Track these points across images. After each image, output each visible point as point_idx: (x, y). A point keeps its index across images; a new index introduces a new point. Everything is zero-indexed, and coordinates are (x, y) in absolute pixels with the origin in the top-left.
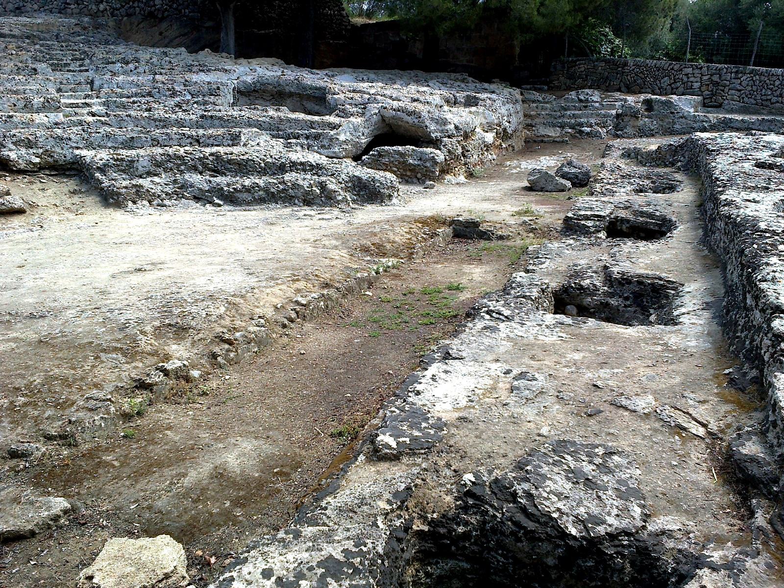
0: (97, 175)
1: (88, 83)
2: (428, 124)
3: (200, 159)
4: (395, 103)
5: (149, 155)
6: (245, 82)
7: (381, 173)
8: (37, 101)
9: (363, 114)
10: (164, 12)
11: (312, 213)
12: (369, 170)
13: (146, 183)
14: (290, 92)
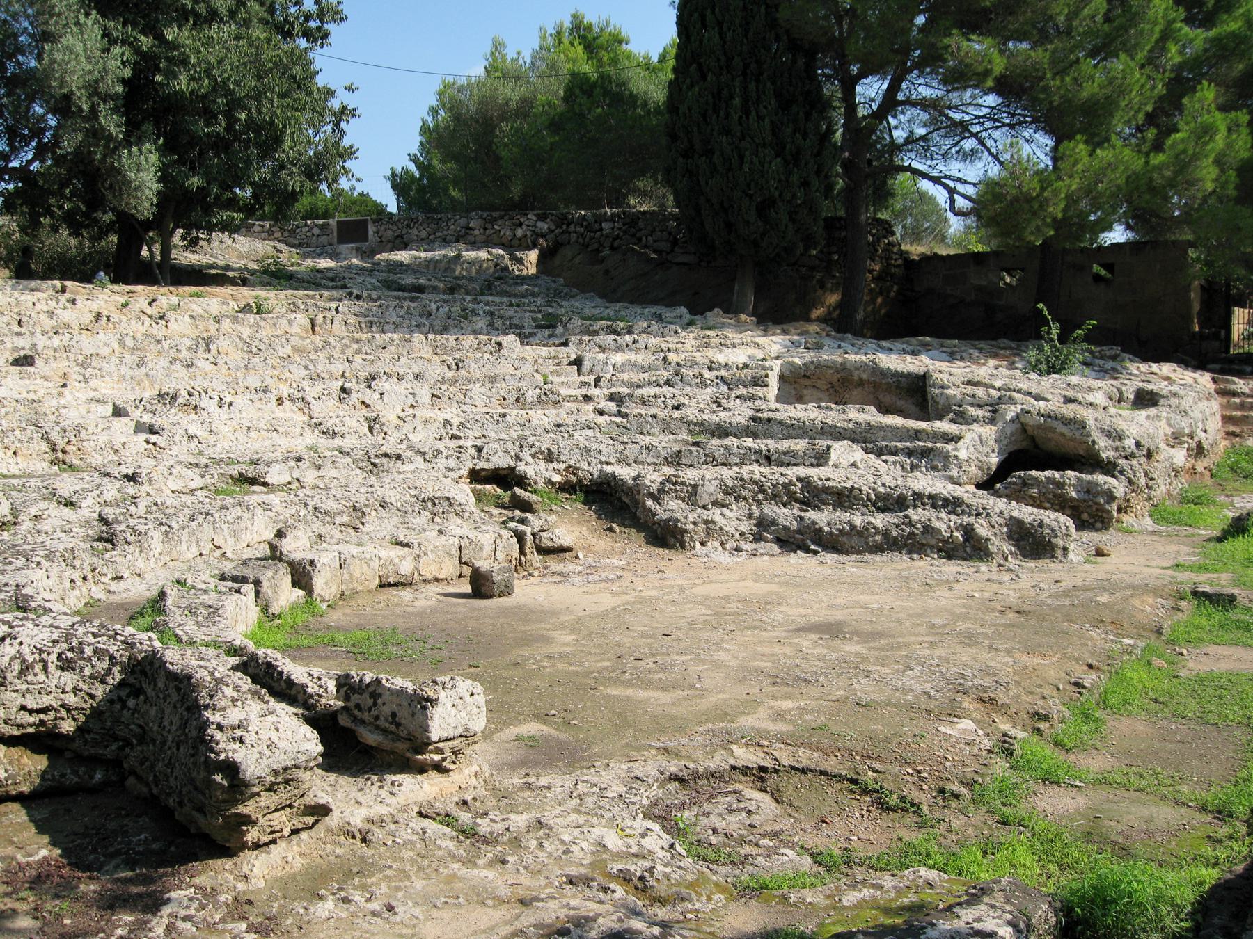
0: (649, 503)
1: (571, 364)
3: (785, 486)
4: (1042, 403)
6: (792, 364)
8: (532, 394)
9: (992, 421)
10: (614, 239)
11: (967, 570)
14: (861, 379)
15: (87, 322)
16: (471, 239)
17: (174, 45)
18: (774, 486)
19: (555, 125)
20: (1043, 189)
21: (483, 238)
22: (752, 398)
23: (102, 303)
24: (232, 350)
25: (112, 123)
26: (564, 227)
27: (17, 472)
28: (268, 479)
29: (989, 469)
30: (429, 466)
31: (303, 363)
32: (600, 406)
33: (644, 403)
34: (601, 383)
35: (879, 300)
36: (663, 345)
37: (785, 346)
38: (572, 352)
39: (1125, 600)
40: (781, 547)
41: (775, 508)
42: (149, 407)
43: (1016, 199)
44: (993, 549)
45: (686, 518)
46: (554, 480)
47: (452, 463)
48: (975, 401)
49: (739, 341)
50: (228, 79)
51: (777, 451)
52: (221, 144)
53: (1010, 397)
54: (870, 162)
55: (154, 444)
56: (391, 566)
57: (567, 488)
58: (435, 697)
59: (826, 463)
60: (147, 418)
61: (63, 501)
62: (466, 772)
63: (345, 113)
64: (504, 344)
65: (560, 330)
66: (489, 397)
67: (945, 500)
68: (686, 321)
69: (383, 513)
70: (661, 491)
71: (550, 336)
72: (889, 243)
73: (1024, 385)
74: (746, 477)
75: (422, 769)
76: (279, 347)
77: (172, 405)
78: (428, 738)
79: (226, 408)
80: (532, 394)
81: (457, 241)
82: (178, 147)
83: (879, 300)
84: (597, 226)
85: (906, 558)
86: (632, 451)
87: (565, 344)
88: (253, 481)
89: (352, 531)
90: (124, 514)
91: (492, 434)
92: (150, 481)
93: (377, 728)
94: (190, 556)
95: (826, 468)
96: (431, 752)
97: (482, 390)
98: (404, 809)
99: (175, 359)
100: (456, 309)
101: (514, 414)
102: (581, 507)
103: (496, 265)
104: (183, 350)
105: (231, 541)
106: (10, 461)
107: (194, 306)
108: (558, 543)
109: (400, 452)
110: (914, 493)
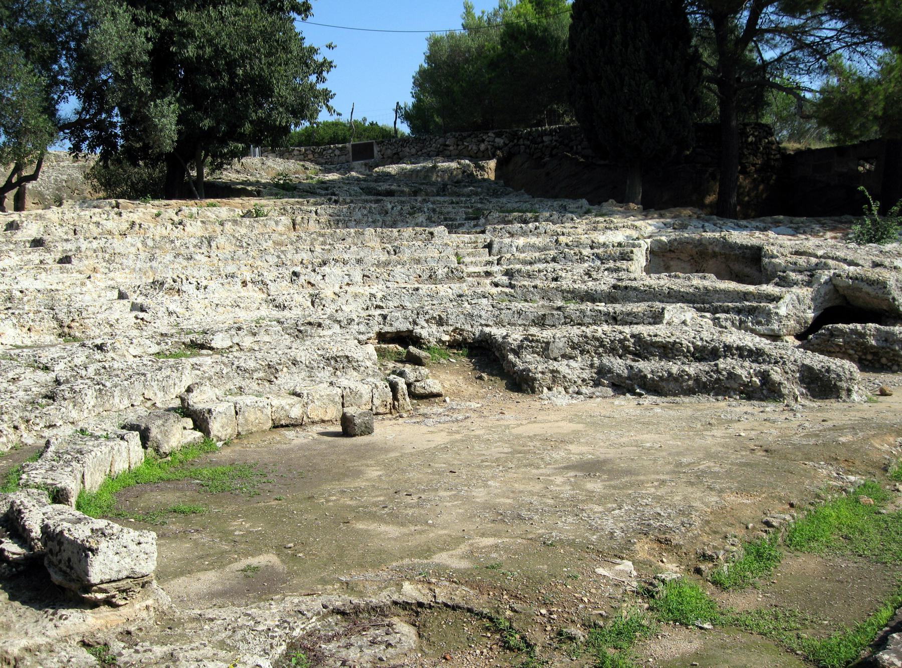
0: (511, 357)
1: (485, 247)
2: (896, 296)
3: (620, 341)
5: (565, 337)
6: (660, 241)
7: (838, 361)
8: (441, 272)
9: (809, 284)
10: (553, 149)
12: (822, 357)
13: (562, 367)
14: (714, 252)
15: (125, 229)
16: (448, 153)
17: (183, 24)
18: (612, 342)
19: (493, 64)
20: (864, 93)
21: (454, 153)
22: (617, 270)
23: (141, 214)
24: (227, 245)
25: (142, 83)
26: (515, 141)
27: (29, 344)
28: (213, 345)
29: (806, 322)
30: (344, 331)
31: (276, 254)
32: (496, 280)
33: (529, 276)
34: (502, 262)
35: (761, 187)
36: (559, 230)
37: (658, 228)
38: (488, 237)
39: (866, 439)
40: (614, 391)
41: (612, 359)
42: (144, 291)
43: (843, 102)
44: (785, 391)
45: (536, 368)
46: (443, 339)
47: (362, 328)
48: (797, 268)
49: (621, 225)
50: (225, 45)
51: (622, 313)
52: (227, 94)
53: (825, 264)
54: (739, 79)
55: (142, 319)
56: (283, 412)
57: (454, 345)
58: (94, 546)
59: (661, 322)
60: (140, 300)
61: (41, 366)
62: (137, 606)
63: (327, 65)
64: (435, 234)
65: (482, 221)
66: (408, 276)
67: (750, 351)
68: (584, 209)
69: (294, 369)
70: (520, 347)
71: (475, 226)
72: (769, 142)
73: (841, 254)
74: (589, 335)
75: (94, 605)
76: (263, 242)
77: (161, 289)
78: (89, 581)
79: (202, 290)
80: (441, 272)
81: (437, 155)
82: (194, 99)
83: (761, 187)
84: (539, 139)
85: (712, 399)
86: (506, 316)
87: (483, 232)
88: (202, 347)
89: (267, 384)
90: (74, 376)
91: (408, 304)
92: (114, 349)
93: (61, 570)
94: (122, 407)
95: (660, 326)
96: (96, 592)
97: (402, 270)
98: (65, 639)
99: (178, 255)
100: (407, 207)
101: (425, 288)
102: (465, 360)
103: (464, 172)
104: (191, 247)
105: (160, 394)
106: (25, 335)
107: (209, 214)
108: (429, 390)
109: (321, 321)
110: (725, 346)
